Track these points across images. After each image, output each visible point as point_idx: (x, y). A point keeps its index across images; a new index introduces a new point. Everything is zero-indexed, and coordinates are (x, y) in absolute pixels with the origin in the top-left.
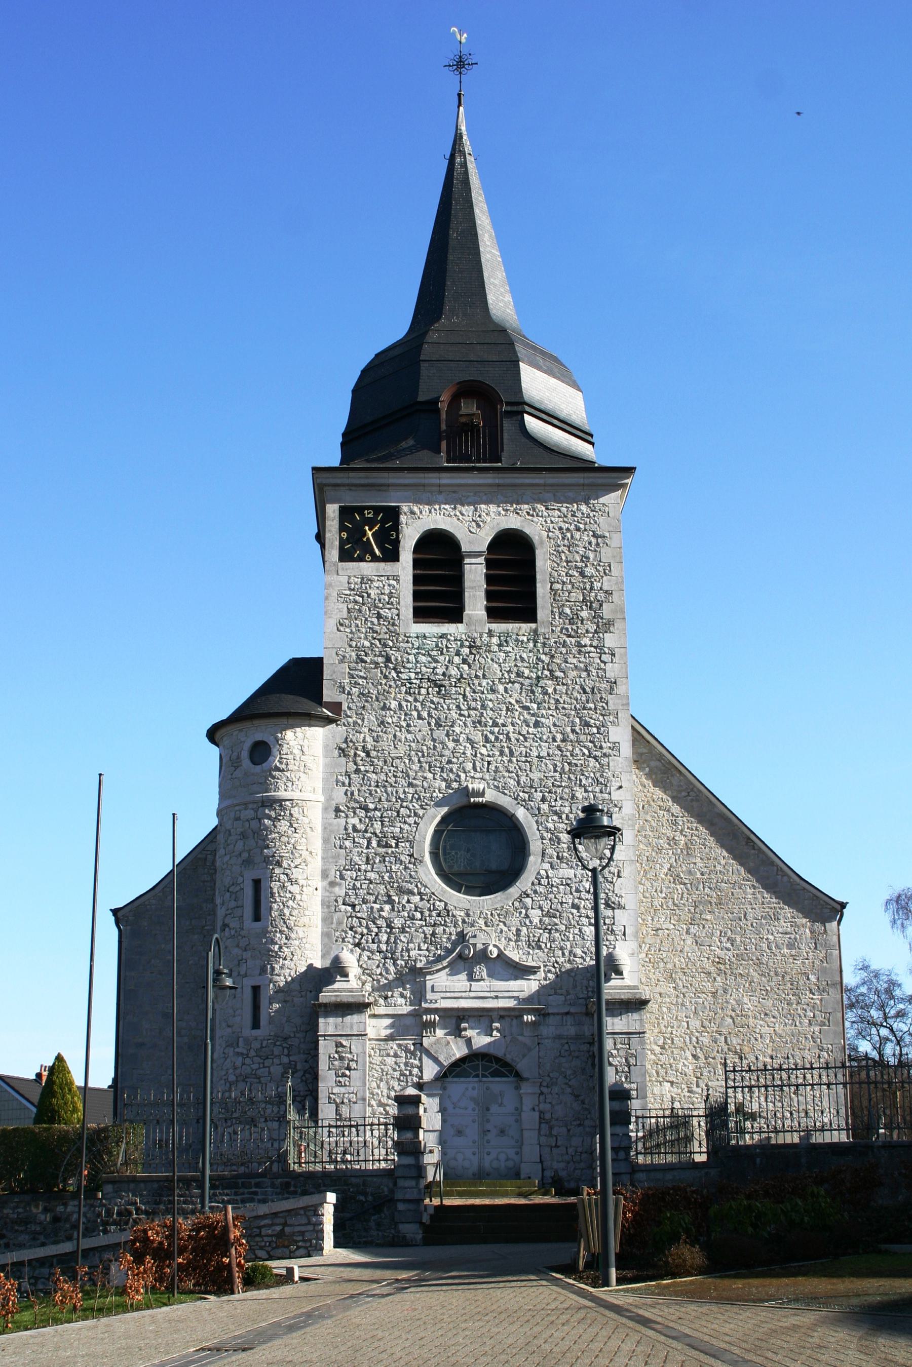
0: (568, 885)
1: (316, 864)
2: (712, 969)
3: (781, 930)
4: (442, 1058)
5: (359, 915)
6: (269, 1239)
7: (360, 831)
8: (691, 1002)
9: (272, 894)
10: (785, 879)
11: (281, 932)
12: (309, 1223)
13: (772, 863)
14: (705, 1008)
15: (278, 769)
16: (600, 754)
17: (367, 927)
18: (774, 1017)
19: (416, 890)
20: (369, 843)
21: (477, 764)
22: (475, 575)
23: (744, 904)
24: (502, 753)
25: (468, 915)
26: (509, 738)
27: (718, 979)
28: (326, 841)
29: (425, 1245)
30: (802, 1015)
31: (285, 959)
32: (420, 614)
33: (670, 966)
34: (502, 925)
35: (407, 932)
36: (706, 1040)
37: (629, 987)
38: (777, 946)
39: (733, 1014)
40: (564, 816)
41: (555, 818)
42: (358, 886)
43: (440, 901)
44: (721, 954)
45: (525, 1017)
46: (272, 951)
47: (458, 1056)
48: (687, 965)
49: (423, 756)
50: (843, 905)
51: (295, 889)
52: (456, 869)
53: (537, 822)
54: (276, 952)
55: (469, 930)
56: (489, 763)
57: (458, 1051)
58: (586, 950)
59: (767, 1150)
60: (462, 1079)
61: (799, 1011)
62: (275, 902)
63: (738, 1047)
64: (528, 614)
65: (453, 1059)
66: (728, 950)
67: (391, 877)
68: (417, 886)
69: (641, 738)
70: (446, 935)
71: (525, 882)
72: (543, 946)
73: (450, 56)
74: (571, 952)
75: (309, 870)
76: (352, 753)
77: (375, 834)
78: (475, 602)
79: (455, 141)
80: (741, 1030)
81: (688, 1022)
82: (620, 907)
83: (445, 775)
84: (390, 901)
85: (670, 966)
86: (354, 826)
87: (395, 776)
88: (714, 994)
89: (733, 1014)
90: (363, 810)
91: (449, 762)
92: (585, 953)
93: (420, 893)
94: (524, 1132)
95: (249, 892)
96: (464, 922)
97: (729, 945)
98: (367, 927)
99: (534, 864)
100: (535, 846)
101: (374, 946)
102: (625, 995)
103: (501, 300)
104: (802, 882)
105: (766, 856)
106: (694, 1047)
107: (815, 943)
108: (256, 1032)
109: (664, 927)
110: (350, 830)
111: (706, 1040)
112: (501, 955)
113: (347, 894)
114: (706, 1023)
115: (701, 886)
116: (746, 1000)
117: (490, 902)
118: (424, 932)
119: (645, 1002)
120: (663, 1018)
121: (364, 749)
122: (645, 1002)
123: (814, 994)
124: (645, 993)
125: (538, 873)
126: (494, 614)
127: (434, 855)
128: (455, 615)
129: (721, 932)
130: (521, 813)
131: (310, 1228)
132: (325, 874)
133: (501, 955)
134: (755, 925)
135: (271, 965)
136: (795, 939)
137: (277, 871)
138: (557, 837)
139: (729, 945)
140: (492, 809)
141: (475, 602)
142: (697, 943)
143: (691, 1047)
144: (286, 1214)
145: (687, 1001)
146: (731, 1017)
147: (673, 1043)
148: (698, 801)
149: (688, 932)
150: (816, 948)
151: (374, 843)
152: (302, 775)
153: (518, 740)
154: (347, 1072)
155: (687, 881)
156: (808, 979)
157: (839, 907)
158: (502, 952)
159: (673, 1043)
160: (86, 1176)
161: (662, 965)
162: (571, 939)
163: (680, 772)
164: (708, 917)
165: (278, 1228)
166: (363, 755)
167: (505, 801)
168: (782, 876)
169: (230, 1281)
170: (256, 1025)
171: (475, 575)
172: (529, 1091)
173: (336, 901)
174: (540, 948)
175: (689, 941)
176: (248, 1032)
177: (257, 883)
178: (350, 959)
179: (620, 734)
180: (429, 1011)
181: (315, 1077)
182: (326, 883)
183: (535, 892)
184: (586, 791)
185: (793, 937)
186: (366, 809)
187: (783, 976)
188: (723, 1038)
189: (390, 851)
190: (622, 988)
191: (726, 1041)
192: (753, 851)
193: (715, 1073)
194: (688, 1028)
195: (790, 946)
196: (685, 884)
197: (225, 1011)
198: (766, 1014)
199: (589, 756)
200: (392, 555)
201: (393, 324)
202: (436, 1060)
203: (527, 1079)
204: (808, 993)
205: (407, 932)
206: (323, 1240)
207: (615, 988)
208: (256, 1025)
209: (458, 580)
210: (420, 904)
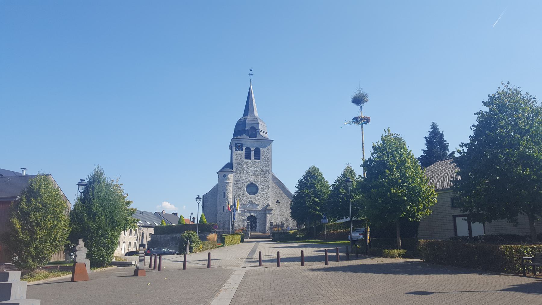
16: (267, 177)
22: (253, 154)
32: (246, 158)
57: (249, 215)
64: (259, 159)
69: (273, 175)
71: (258, 193)
73: (354, 93)
78: (253, 157)
79: (158, 217)
90: (237, 182)
99: (259, 191)
103: (256, 114)
126: (255, 159)
128: (250, 159)
140: (254, 184)
141: (253, 157)
171: (253, 154)
176: (222, 212)
179: (270, 175)
197: (220, 208)
200: (242, 150)
201: (240, 115)
209: (250, 154)
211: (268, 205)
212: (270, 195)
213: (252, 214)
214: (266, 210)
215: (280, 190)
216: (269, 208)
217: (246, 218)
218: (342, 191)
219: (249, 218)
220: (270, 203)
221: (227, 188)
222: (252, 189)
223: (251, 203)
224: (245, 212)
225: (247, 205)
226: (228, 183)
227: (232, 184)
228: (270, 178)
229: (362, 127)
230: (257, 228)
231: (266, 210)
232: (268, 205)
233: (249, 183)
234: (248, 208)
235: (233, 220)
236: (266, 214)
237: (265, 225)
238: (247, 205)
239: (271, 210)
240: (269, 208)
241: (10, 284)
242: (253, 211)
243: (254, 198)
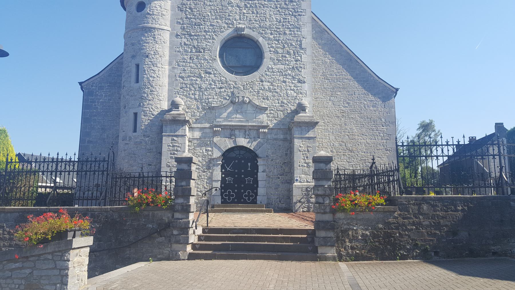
1: (166, 58)
2: (340, 115)
3: (370, 100)
6: (19, 282)
7: (188, 45)
9: (144, 71)
11: (148, 88)
12: (55, 268)
13: (365, 71)
15: (149, 14)
20: (191, 50)
21: (242, 17)
24: (253, 13)
25: (236, 84)
26: (256, 7)
27: (343, 119)
28: (171, 48)
29: (188, 259)
33: (322, 113)
36: (337, 144)
37: (308, 116)
38: (368, 107)
40: (280, 41)
41: (277, 43)
43: (224, 77)
47: (230, 147)
49: (217, 12)
50: (397, 90)
51: (155, 68)
52: (231, 65)
53: (268, 44)
54: (145, 97)
56: (247, 17)
57: (229, 144)
63: (351, 148)
64: (317, 160)
65: (227, 148)
67: (201, 66)
71: (262, 69)
74: (282, 102)
75: (163, 59)
76: (184, 9)
77: (194, 46)
82: (304, 82)
83: (227, 21)
85: (322, 113)
86: (185, 43)
87: (204, 21)
91: (229, 16)
94: (211, 225)
95: (134, 70)
97: (347, 105)
98: (190, 88)
99: (267, 62)
100: (267, 55)
102: (307, 120)
104: (380, 80)
105: (364, 68)
108: (135, 134)
110: (183, 44)
111: (337, 144)
113: (181, 73)
115: (336, 81)
116: (354, 128)
118: (216, 91)
121: (190, 8)
124: (316, 119)
125: (268, 67)
127: (221, 56)
130: (261, 40)
131: (56, 272)
132: (170, 63)
137: (147, 59)
138: (276, 51)
139: (347, 105)
143: (330, 147)
144: (37, 258)
146: (348, 135)
148: (335, 45)
149: (330, 100)
151: (194, 50)
152: (160, 17)
153: (260, 7)
154: (176, 153)
156: (381, 120)
157: (395, 90)
161: (318, 113)
163: (328, 33)
165: (28, 271)
166: (190, 11)
167: (254, 34)
170: (135, 131)
173: (175, 76)
174: (268, 100)
175: (330, 103)
176: (131, 134)
177: (138, 66)
178: (179, 100)
181: (160, 153)
182: (171, 67)
183: (266, 75)
184: (290, 31)
186: (190, 35)
188: (344, 144)
189: (201, 54)
190: (305, 117)
197: (126, 121)
198: (363, 134)
199: (292, 15)
202: (219, 149)
203: (261, 158)
206: (67, 285)
208: (135, 131)
210: (214, 78)
211: (301, 108)
212: (306, 73)
213: (243, 142)
215: (337, 68)
216: (302, 117)
217: (217, 154)
220: (306, 102)
221: (149, 48)
222: (242, 53)
223: (237, 104)
224: (215, 134)
226: (150, 29)
227: (166, 36)
228: (307, 31)
229: (208, 216)
230: (261, 191)
231: (292, 126)
232: (301, 108)
233: (228, 32)
235: (65, 191)
236: (291, 142)
237: (290, 181)
239: (312, 125)
240: (302, 117)
242: (245, 130)
243: (249, 87)
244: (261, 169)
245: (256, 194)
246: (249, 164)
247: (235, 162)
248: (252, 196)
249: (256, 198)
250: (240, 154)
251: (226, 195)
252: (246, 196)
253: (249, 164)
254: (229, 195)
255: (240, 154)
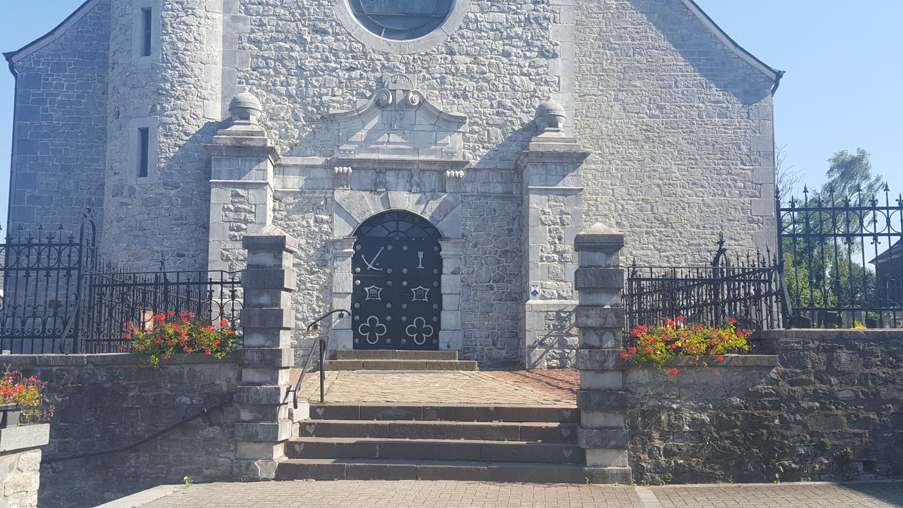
0: (498, 29)
2: (640, 137)
3: (712, 99)
4: (354, 214)
5: (266, 54)
8: (616, 169)
9: (164, 25)
10: (719, 46)
14: (632, 175)
17: (275, 69)
18: (702, 187)
19: (330, 30)
23: (674, 71)
25: (388, 60)
27: (646, 146)
30: (732, 186)
31: (178, 99)
34: (424, 72)
35: (320, 76)
36: (631, 208)
38: (708, 116)
39: (661, 182)
42: (266, 21)
43: (358, 42)
44: (650, 121)
45: (448, 172)
46: (162, 89)
47: (373, 212)
48: (614, 132)
50: (779, 75)
51: (190, 19)
52: (376, 11)
54: (167, 91)
55: (388, 76)
57: (369, 205)
58: (516, 101)
59: (279, 335)
60: (514, 406)
61: (729, 182)
62: (168, 34)
63: (665, 216)
65: (367, 216)
66: (658, 117)
68: (331, 26)
70: (365, 80)
72: (470, 95)
80: (669, 199)
81: (613, 190)
82: (555, 56)
84: (302, 42)
88: (641, 162)
89: (661, 182)
92: (515, 105)
93: (335, 34)
96: (383, 67)
97: (657, 112)
101: (283, 90)
102: (561, 147)
105: (700, 22)
106: (619, 215)
107: (748, 113)
109: (592, 92)
111: (631, 208)
112: (422, 102)
113: (253, 32)
114: (633, 191)
116: (674, 168)
117: (412, 46)
119: (585, 155)
120: (588, 185)
122: (585, 155)
123: (744, 164)
124: (583, 145)
125: (467, 17)
129: (650, 99)
133: (422, 102)
134: (685, 92)
135: (161, 105)
136: (727, 108)
142: (625, 109)
143: (616, 214)
145: (613, 167)
146: (658, 186)
147: (597, 210)
149: (616, 99)
150: (748, 118)
155: (616, 46)
157: (774, 76)
158: (424, 100)
159: (597, 210)
160: (870, 323)
162: (501, 89)
164: (638, 84)
168: (717, 44)
169: (276, 389)
170: (143, 172)
172: (451, 253)
173: (240, 38)
174: (466, 98)
176: (133, 179)
180: (342, 163)
183: (462, 36)
185: (725, 105)
187: (713, 146)
188: (649, 207)
190: (555, 140)
191: (652, 210)
192: (686, 18)
193: (640, 242)
194: (613, 196)
195: (721, 115)
196: (615, 49)
197: (121, 149)
202: (348, 217)
204: (739, 163)
205: (320, 76)
207: (548, 139)
208: (143, 172)
212: (558, 34)
213: (405, 200)
214: (524, 163)
216: (548, 140)
217: (343, 230)
218: (300, 352)
219: (373, 237)
220: (558, 104)
223: (393, 109)
224: (338, 181)
225: (359, 117)
230: (449, 319)
231: (524, 163)
232: (547, 118)
234: (365, 145)
236: (520, 202)
238: (359, 117)
239: (573, 160)
240: (548, 140)
241: (281, 350)
242: (409, 173)
244: (448, 266)
245: (438, 327)
246: (421, 255)
247: (386, 248)
248: (427, 331)
249: (436, 335)
250: (397, 231)
251: (364, 329)
252: (412, 331)
253: (421, 255)
254: (373, 329)
255: (397, 231)
